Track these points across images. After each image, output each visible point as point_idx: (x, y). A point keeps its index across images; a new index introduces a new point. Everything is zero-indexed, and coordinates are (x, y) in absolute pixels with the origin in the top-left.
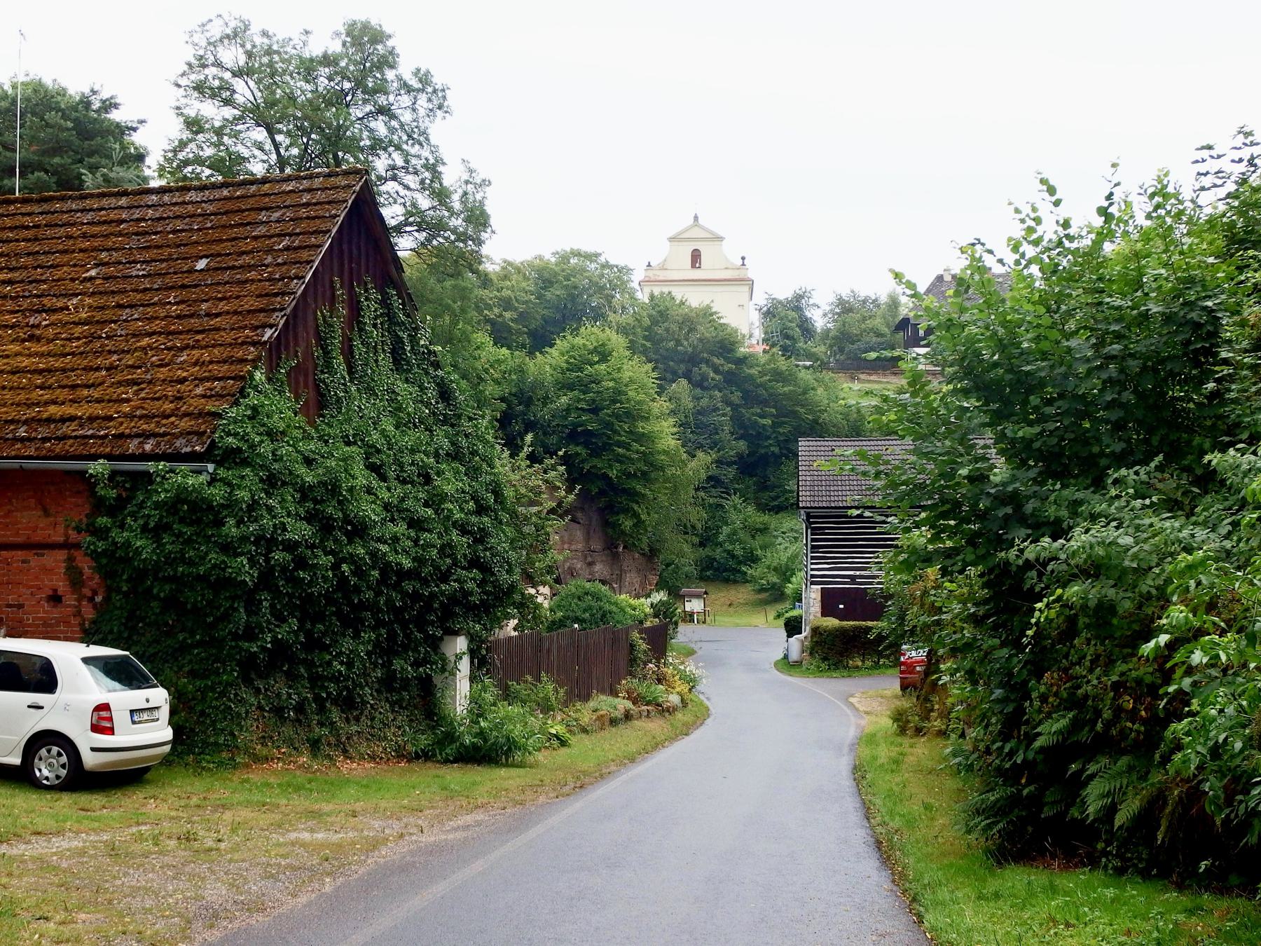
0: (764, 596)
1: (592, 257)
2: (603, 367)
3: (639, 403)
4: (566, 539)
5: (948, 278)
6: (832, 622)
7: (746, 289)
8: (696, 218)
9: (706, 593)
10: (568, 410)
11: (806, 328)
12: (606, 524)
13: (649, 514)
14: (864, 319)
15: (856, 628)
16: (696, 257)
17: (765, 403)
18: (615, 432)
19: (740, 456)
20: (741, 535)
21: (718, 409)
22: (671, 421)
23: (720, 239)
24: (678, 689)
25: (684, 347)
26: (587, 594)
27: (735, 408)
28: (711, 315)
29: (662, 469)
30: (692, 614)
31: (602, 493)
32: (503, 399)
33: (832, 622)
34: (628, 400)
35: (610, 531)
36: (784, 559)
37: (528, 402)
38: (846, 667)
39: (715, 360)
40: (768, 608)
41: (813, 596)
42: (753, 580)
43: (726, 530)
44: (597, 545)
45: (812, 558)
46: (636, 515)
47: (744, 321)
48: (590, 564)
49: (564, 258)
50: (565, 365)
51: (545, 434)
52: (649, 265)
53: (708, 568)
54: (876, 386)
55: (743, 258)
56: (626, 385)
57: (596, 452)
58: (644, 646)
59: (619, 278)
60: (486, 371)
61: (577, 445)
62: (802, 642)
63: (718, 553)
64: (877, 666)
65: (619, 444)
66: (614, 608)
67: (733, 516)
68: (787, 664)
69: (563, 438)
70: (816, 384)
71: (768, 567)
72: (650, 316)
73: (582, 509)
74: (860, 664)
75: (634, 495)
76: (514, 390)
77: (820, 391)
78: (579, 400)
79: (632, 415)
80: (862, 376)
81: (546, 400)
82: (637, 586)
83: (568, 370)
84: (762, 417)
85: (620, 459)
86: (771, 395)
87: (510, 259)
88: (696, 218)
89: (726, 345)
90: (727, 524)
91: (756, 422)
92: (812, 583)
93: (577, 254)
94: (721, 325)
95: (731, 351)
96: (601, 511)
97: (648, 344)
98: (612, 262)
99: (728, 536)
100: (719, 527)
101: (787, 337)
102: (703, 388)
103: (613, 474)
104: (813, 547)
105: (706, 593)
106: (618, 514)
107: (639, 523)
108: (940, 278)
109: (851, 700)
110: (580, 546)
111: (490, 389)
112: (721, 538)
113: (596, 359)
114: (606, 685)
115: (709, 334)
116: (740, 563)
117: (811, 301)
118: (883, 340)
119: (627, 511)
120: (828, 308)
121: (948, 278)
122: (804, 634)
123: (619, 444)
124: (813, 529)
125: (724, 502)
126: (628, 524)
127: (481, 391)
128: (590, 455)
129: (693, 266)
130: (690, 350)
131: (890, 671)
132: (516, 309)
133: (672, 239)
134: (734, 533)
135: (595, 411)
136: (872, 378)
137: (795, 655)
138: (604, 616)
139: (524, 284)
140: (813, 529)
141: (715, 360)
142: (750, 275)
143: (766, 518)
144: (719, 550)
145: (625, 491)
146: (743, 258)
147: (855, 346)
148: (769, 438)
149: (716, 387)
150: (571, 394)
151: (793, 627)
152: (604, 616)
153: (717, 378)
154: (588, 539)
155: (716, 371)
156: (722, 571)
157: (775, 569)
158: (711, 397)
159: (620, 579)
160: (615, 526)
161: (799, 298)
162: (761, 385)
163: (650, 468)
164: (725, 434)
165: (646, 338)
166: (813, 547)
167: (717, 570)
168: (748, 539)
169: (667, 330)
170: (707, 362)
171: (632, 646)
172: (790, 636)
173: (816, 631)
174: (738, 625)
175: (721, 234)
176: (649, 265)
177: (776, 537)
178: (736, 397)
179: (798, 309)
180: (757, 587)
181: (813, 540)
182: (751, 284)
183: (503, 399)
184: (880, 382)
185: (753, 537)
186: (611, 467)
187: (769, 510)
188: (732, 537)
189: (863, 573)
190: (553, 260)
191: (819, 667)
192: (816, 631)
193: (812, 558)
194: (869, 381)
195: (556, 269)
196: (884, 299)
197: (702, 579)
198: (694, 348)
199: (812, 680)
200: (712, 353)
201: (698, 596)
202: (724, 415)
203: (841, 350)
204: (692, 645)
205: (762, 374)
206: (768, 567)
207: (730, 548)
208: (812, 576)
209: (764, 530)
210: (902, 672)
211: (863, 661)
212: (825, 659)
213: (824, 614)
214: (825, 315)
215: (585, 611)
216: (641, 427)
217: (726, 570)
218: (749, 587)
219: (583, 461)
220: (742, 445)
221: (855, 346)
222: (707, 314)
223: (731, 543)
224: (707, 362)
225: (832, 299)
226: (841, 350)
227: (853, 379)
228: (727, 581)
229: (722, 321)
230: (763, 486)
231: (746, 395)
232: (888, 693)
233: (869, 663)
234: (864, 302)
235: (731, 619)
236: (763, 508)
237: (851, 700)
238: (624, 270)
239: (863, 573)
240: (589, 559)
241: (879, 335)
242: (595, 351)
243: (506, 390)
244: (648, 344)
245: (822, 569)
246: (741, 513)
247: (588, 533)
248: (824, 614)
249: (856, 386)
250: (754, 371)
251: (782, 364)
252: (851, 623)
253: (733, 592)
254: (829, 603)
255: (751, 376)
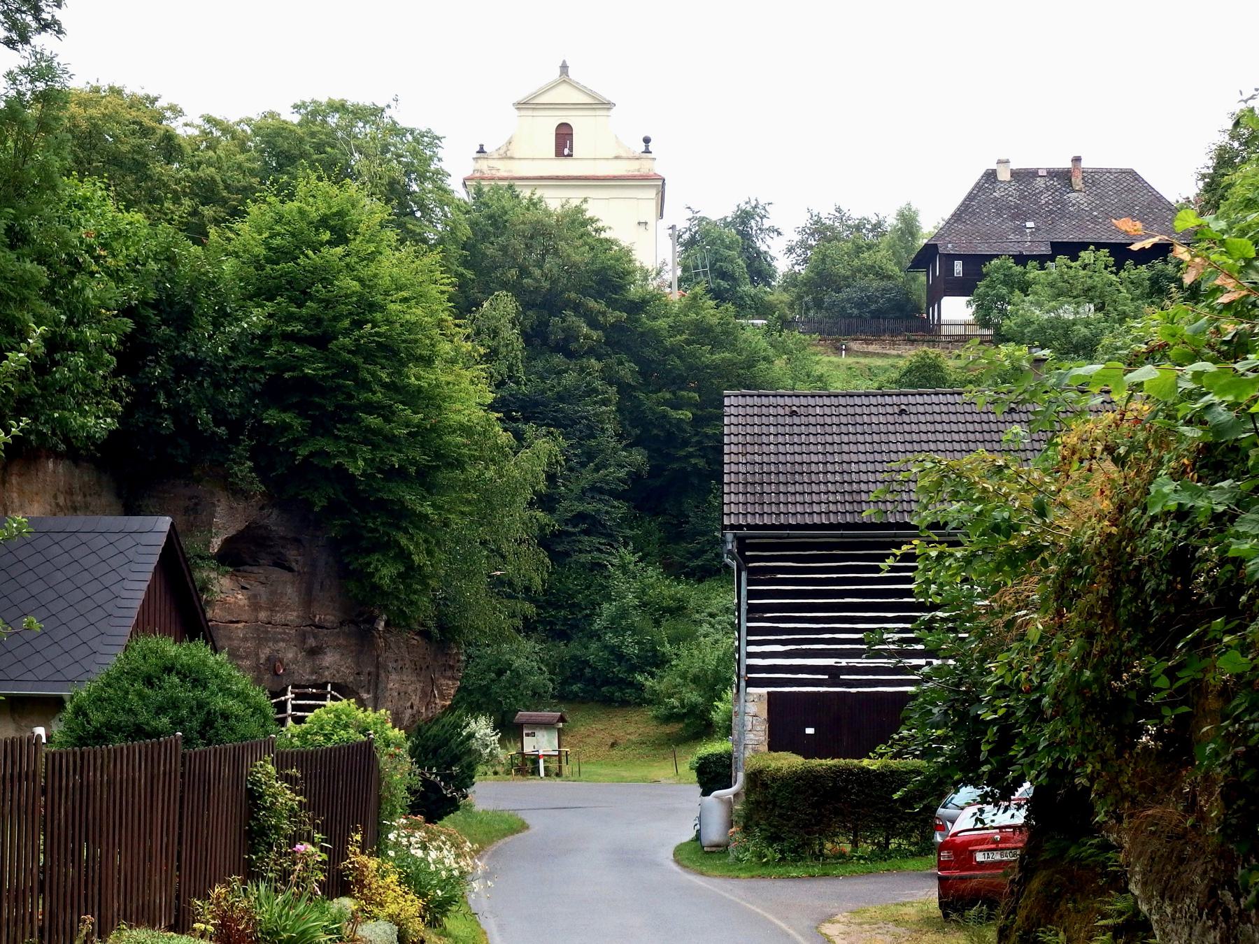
0: (675, 728)
1: (371, 114)
2: (339, 250)
3: (411, 327)
4: (263, 600)
5: (1004, 175)
6: (789, 761)
7: (652, 193)
8: (564, 68)
9: (562, 719)
10: (266, 338)
11: (759, 269)
12: (345, 573)
13: (430, 553)
14: (859, 250)
15: (837, 772)
16: (564, 136)
17: (679, 382)
18: (364, 385)
19: (635, 477)
20: (636, 618)
21: (595, 391)
22: (479, 370)
23: (607, 105)
24: (392, 908)
25: (544, 287)
26: (169, 670)
27: (624, 389)
28: (584, 224)
29: (459, 464)
30: (535, 760)
31: (335, 508)
32: (127, 311)
33: (789, 761)
34: (389, 322)
35: (352, 585)
36: (711, 660)
37: (182, 318)
38: (819, 856)
39: (592, 303)
40: (681, 751)
41: (751, 709)
42: (654, 700)
43: (608, 609)
44: (327, 615)
45: (751, 631)
46: (403, 556)
47: (650, 247)
48: (314, 652)
49: (313, 113)
50: (261, 251)
51: (217, 385)
52: (481, 151)
53: (575, 678)
54: (879, 362)
55: (647, 141)
56: (387, 293)
57: (321, 425)
58: (287, 797)
59: (415, 153)
60: (90, 249)
61: (285, 410)
62: (729, 804)
63: (593, 652)
64: (883, 853)
65: (370, 408)
66: (233, 705)
67: (619, 583)
68: (700, 854)
69: (256, 394)
70: (771, 352)
71: (683, 676)
72: (474, 224)
73: (297, 541)
74: (848, 848)
75: (401, 516)
76: (152, 295)
77: (780, 363)
78: (290, 318)
79: (394, 352)
80: (855, 346)
81: (221, 317)
82: (415, 699)
83: (269, 260)
84: (676, 407)
85: (371, 438)
86: (691, 368)
87: (217, 115)
88: (564, 68)
89: (609, 276)
90: (609, 599)
91: (664, 416)
92: (752, 683)
93: (341, 108)
94: (600, 241)
95: (621, 288)
96: (334, 546)
97: (469, 274)
98: (403, 123)
99: (612, 621)
100: (594, 605)
101: (723, 275)
102: (570, 355)
103: (357, 467)
104: (752, 609)
105: (562, 719)
106: (369, 551)
107: (411, 571)
108: (991, 176)
109: (828, 929)
110: (292, 616)
111: (95, 289)
112: (598, 624)
113: (326, 236)
114: (161, 899)
115: (580, 256)
116: (633, 669)
117: (767, 223)
118: (890, 284)
119: (385, 546)
120: (797, 238)
121: (1004, 175)
122: (734, 789)
123: (370, 408)
124: (752, 571)
125: (604, 559)
126: (386, 573)
127: (76, 291)
128: (312, 432)
129: (559, 153)
130: (546, 285)
131: (912, 864)
132: (224, 202)
133: (522, 105)
134: (623, 613)
135: (321, 341)
136: (871, 348)
137: (714, 833)
138: (208, 723)
139: (241, 158)
140: (752, 571)
141: (592, 303)
142: (658, 168)
143: (681, 589)
144: (594, 646)
145: (382, 505)
146: (647, 141)
147: (843, 295)
148: (686, 443)
149: (591, 352)
150: (270, 307)
151: (713, 775)
152: (208, 723)
153: (595, 335)
154: (308, 601)
155: (593, 324)
156: (599, 686)
157: (696, 680)
158: (582, 370)
159: (375, 684)
160: (362, 576)
161: (745, 217)
162: (672, 350)
163: (434, 462)
164: (608, 438)
165: (465, 263)
166: (752, 609)
167: (592, 681)
168: (648, 625)
169: (504, 249)
170: (577, 308)
171: (253, 798)
172: (706, 793)
173: (754, 778)
174: (622, 780)
175: (609, 97)
176: (481, 151)
177: (699, 623)
178: (627, 371)
179: (746, 236)
180: (663, 710)
181: (751, 595)
182: (660, 185)
183: (127, 311)
184: (886, 356)
185: (657, 623)
186: (352, 454)
187: (687, 576)
188: (616, 624)
189: (854, 662)
190: (296, 119)
191: (760, 856)
192: (754, 778)
193: (751, 631)
194: (866, 354)
195: (299, 131)
196: (891, 221)
197: (563, 697)
198: (554, 282)
199: (743, 883)
200: (584, 291)
201: (547, 726)
202: (605, 402)
203: (818, 304)
204: (521, 815)
205: (675, 329)
206: (683, 676)
207: (615, 641)
208: (751, 669)
209: (677, 610)
210: (942, 866)
211: (855, 844)
212: (773, 839)
213: (773, 747)
214: (790, 250)
215: (161, 710)
216: (415, 376)
217: (607, 682)
218: (651, 712)
219: (296, 442)
220: (638, 457)
221: (843, 295)
222: (576, 221)
223: (616, 633)
224: (577, 308)
225: (804, 220)
226: (818, 304)
227: (838, 350)
228: (608, 703)
229: (603, 235)
230: (676, 534)
231: (646, 369)
232: (911, 912)
233: (867, 847)
234: (858, 228)
235: (614, 771)
236: (674, 570)
237: (828, 929)
238: (425, 142)
239: (854, 662)
240: (312, 642)
241: (882, 275)
242: (324, 222)
243: (133, 291)
244: (469, 274)
245: (767, 653)
246: (633, 579)
247: (309, 591)
248: (773, 747)
249: (844, 359)
250: (662, 323)
251: (711, 312)
252: (830, 762)
253: (618, 721)
254: (785, 722)
255: (655, 333)
